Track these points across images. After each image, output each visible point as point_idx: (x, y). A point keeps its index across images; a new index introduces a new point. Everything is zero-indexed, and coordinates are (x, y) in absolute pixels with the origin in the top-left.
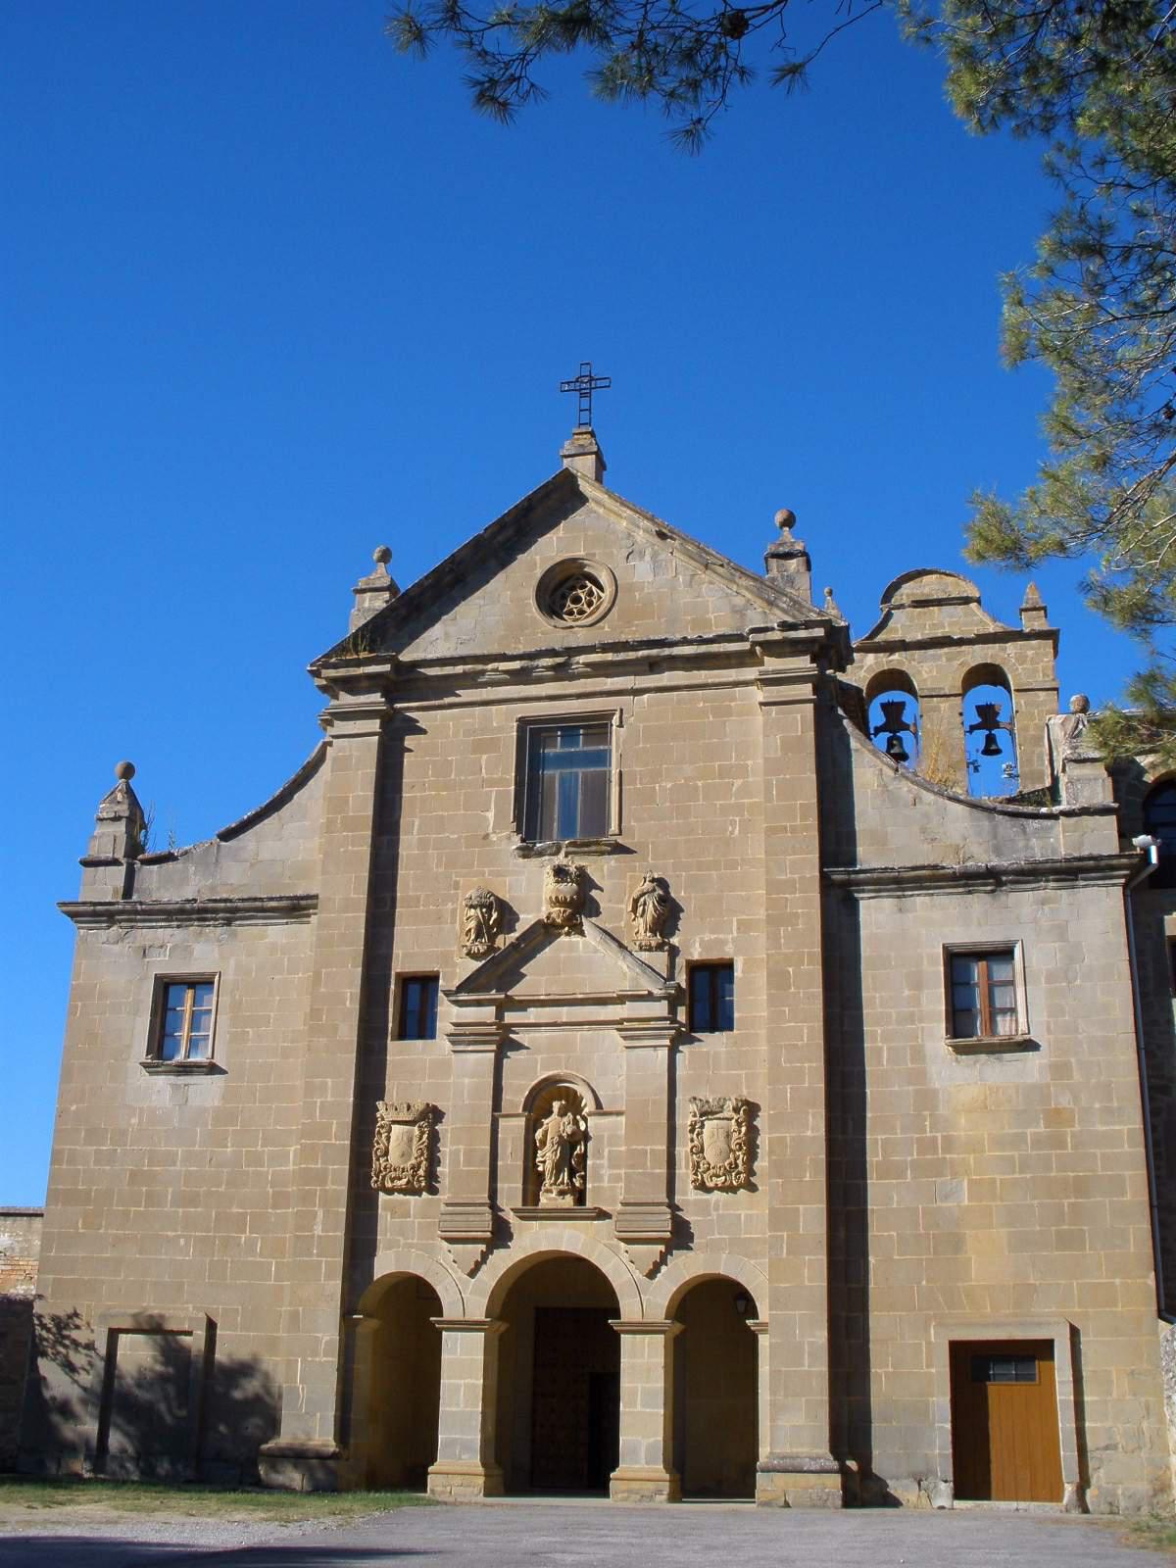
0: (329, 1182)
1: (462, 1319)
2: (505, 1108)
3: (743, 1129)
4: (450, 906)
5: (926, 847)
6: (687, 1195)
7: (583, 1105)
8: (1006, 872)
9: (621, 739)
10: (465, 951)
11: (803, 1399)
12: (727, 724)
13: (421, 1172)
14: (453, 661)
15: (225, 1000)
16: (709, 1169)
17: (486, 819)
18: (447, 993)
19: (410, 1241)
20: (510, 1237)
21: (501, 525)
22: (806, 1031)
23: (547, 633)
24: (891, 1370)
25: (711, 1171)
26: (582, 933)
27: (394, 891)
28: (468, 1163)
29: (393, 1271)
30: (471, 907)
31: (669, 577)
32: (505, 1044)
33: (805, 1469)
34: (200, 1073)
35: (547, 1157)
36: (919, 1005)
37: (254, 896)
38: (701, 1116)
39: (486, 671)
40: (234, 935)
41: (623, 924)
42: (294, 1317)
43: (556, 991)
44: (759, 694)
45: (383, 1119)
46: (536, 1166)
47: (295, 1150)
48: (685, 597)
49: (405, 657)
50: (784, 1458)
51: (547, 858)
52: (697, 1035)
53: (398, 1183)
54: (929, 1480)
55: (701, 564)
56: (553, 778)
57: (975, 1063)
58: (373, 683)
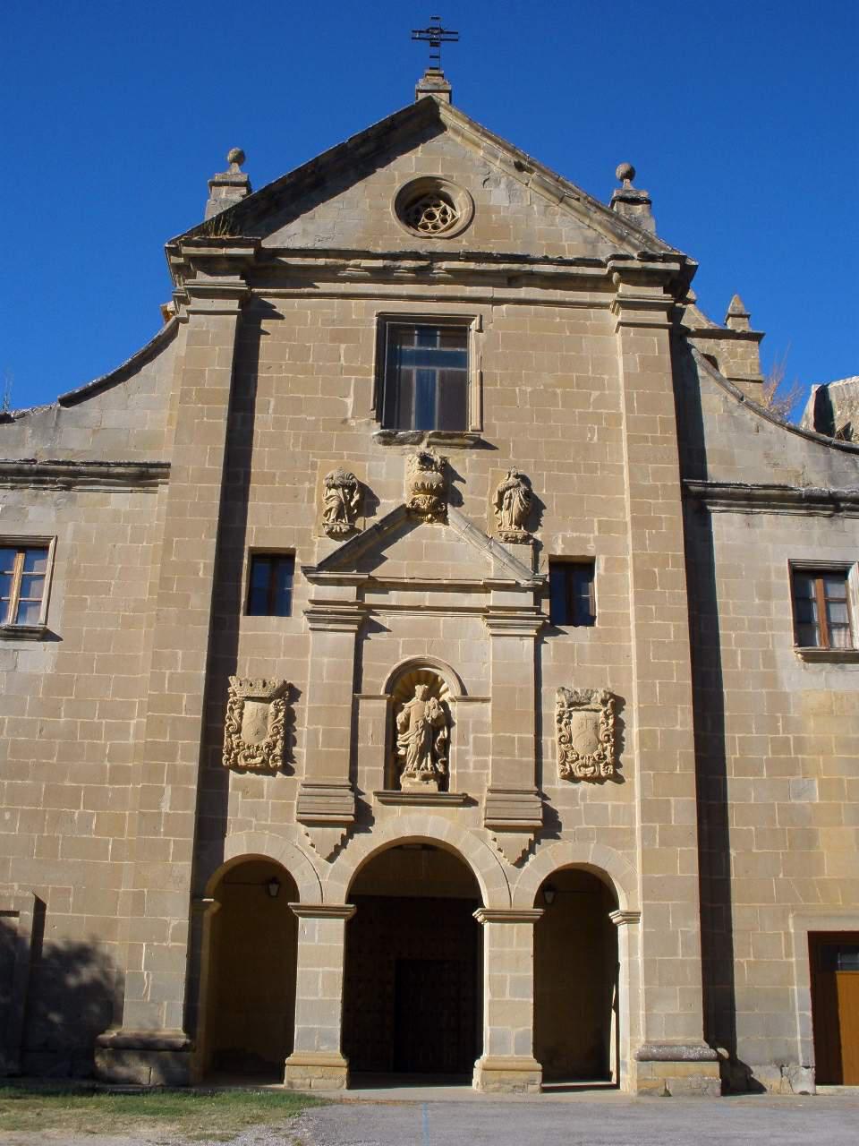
0: (178, 758)
1: (320, 904)
2: (365, 690)
3: (611, 721)
4: (307, 485)
5: (769, 470)
6: (555, 783)
7: (442, 690)
8: (845, 499)
9: (481, 344)
10: (326, 529)
11: (678, 988)
12: (583, 340)
13: (277, 751)
14: (316, 253)
15: (62, 566)
16: (577, 759)
17: (345, 405)
18: (306, 570)
19: (263, 822)
20: (372, 821)
21: (364, 138)
22: (672, 630)
23: (403, 238)
24: (752, 959)
25: (580, 762)
26: (445, 521)
27: (249, 467)
28: (327, 743)
29: (245, 853)
30: (334, 486)
31: (525, 204)
32: (366, 626)
33: (684, 1057)
34: (32, 639)
35: (410, 742)
36: (768, 614)
37: (100, 460)
38: (569, 707)
39: (348, 266)
40: (73, 500)
41: (485, 516)
42: (138, 898)
43: (419, 575)
44: (624, 315)
45: (235, 695)
46: (396, 749)
47: (138, 725)
48: (539, 225)
49: (268, 243)
50: (660, 1047)
51: (408, 446)
52: (563, 628)
53: (253, 761)
54: (790, 1066)
55: (558, 197)
56: (409, 374)
57: (821, 670)
58: (233, 265)
